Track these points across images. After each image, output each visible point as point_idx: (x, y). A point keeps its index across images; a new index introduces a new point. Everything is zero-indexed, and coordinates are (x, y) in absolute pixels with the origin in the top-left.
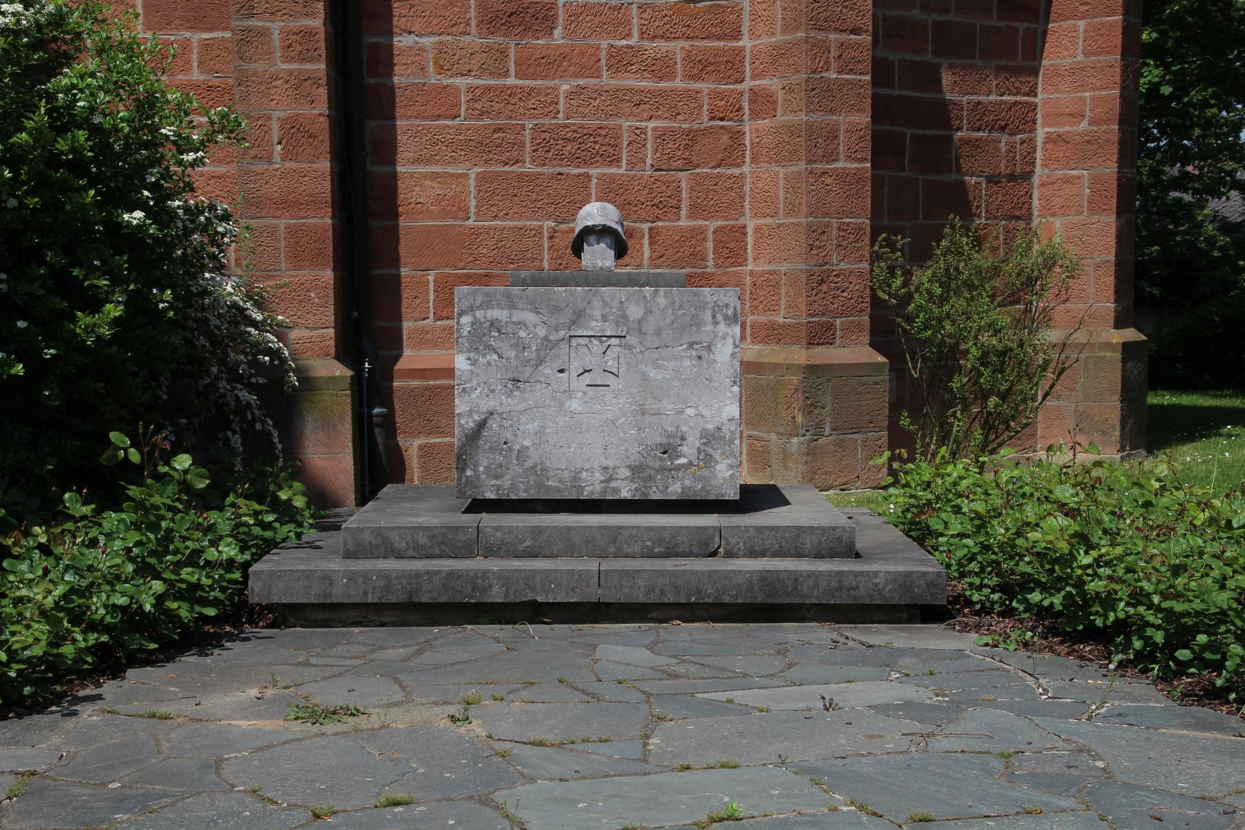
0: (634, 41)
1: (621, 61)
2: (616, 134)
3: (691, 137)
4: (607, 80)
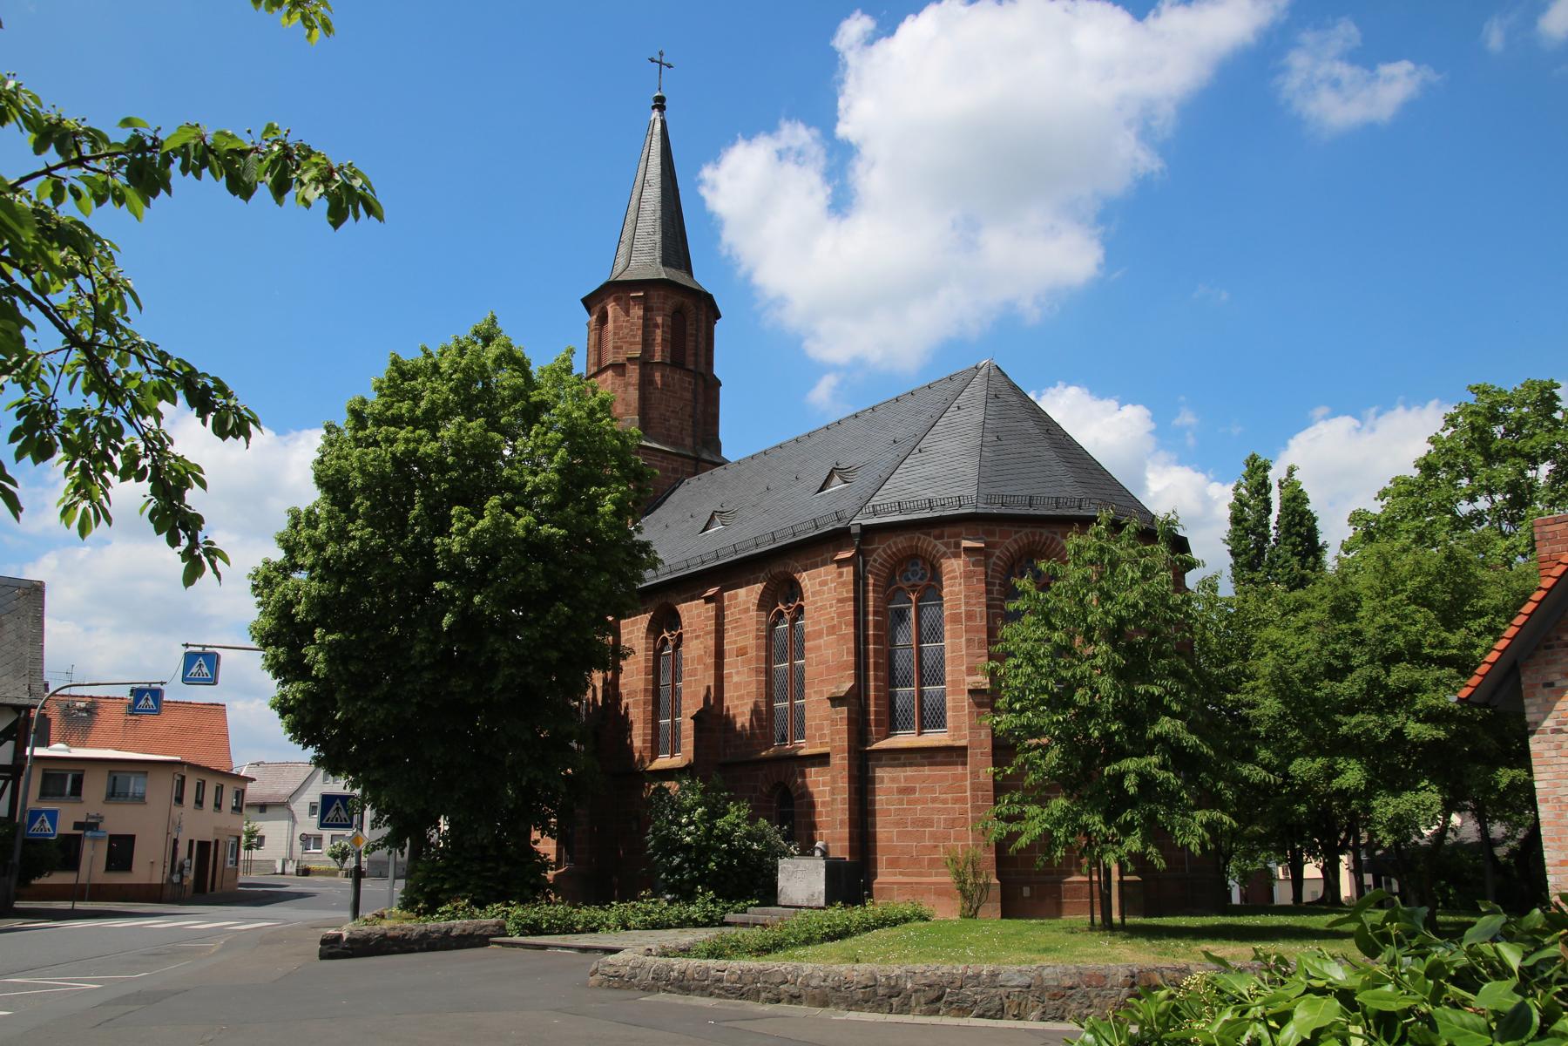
1: (934, 800)
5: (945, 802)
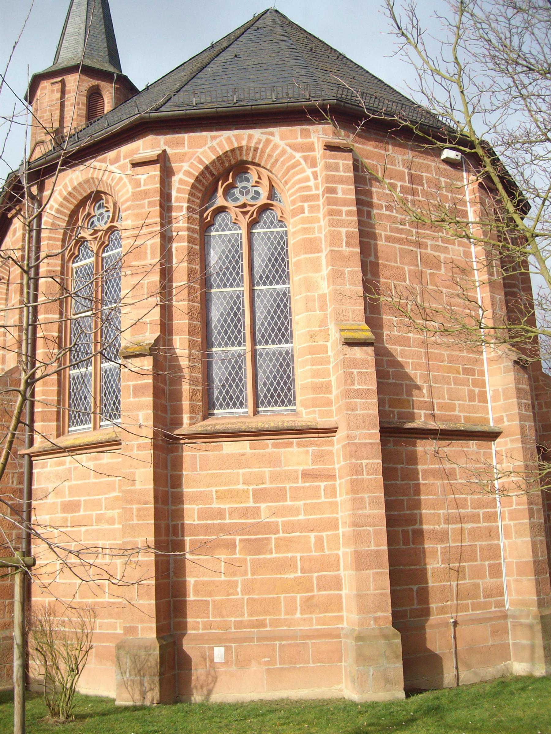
1: (100, 519)
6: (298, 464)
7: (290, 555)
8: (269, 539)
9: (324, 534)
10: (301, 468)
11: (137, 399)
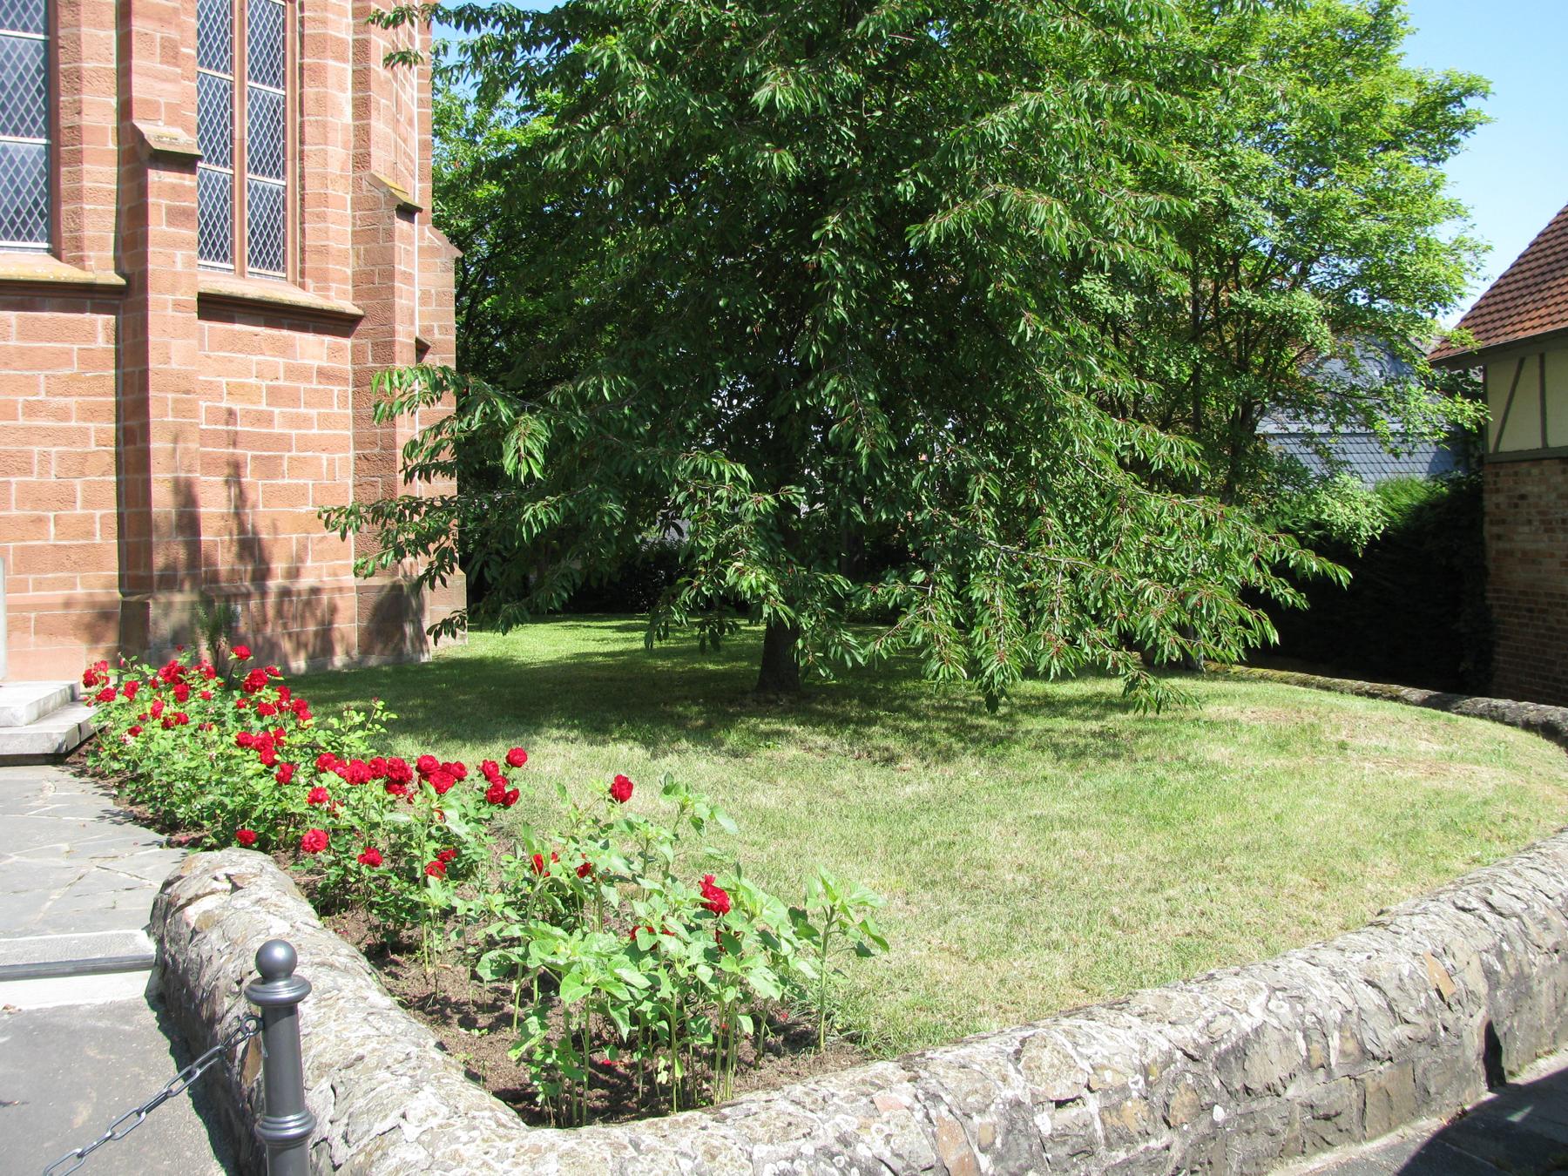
0: (42, 397)
1: (31, 410)
2: (29, 455)
3: (84, 457)
4: (22, 421)
5: (63, 414)
6: (314, 358)
7: (302, 481)
8: (281, 457)
9: (336, 456)
10: (316, 363)
11: (172, 229)
